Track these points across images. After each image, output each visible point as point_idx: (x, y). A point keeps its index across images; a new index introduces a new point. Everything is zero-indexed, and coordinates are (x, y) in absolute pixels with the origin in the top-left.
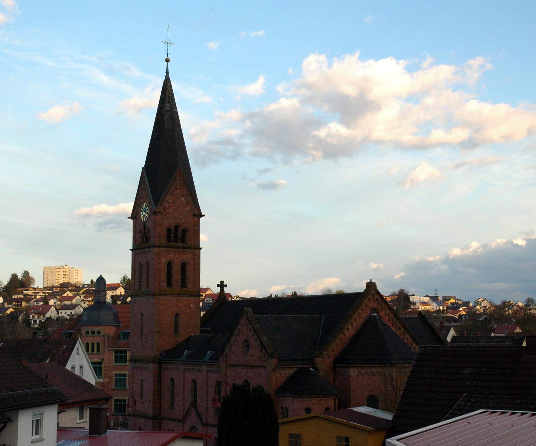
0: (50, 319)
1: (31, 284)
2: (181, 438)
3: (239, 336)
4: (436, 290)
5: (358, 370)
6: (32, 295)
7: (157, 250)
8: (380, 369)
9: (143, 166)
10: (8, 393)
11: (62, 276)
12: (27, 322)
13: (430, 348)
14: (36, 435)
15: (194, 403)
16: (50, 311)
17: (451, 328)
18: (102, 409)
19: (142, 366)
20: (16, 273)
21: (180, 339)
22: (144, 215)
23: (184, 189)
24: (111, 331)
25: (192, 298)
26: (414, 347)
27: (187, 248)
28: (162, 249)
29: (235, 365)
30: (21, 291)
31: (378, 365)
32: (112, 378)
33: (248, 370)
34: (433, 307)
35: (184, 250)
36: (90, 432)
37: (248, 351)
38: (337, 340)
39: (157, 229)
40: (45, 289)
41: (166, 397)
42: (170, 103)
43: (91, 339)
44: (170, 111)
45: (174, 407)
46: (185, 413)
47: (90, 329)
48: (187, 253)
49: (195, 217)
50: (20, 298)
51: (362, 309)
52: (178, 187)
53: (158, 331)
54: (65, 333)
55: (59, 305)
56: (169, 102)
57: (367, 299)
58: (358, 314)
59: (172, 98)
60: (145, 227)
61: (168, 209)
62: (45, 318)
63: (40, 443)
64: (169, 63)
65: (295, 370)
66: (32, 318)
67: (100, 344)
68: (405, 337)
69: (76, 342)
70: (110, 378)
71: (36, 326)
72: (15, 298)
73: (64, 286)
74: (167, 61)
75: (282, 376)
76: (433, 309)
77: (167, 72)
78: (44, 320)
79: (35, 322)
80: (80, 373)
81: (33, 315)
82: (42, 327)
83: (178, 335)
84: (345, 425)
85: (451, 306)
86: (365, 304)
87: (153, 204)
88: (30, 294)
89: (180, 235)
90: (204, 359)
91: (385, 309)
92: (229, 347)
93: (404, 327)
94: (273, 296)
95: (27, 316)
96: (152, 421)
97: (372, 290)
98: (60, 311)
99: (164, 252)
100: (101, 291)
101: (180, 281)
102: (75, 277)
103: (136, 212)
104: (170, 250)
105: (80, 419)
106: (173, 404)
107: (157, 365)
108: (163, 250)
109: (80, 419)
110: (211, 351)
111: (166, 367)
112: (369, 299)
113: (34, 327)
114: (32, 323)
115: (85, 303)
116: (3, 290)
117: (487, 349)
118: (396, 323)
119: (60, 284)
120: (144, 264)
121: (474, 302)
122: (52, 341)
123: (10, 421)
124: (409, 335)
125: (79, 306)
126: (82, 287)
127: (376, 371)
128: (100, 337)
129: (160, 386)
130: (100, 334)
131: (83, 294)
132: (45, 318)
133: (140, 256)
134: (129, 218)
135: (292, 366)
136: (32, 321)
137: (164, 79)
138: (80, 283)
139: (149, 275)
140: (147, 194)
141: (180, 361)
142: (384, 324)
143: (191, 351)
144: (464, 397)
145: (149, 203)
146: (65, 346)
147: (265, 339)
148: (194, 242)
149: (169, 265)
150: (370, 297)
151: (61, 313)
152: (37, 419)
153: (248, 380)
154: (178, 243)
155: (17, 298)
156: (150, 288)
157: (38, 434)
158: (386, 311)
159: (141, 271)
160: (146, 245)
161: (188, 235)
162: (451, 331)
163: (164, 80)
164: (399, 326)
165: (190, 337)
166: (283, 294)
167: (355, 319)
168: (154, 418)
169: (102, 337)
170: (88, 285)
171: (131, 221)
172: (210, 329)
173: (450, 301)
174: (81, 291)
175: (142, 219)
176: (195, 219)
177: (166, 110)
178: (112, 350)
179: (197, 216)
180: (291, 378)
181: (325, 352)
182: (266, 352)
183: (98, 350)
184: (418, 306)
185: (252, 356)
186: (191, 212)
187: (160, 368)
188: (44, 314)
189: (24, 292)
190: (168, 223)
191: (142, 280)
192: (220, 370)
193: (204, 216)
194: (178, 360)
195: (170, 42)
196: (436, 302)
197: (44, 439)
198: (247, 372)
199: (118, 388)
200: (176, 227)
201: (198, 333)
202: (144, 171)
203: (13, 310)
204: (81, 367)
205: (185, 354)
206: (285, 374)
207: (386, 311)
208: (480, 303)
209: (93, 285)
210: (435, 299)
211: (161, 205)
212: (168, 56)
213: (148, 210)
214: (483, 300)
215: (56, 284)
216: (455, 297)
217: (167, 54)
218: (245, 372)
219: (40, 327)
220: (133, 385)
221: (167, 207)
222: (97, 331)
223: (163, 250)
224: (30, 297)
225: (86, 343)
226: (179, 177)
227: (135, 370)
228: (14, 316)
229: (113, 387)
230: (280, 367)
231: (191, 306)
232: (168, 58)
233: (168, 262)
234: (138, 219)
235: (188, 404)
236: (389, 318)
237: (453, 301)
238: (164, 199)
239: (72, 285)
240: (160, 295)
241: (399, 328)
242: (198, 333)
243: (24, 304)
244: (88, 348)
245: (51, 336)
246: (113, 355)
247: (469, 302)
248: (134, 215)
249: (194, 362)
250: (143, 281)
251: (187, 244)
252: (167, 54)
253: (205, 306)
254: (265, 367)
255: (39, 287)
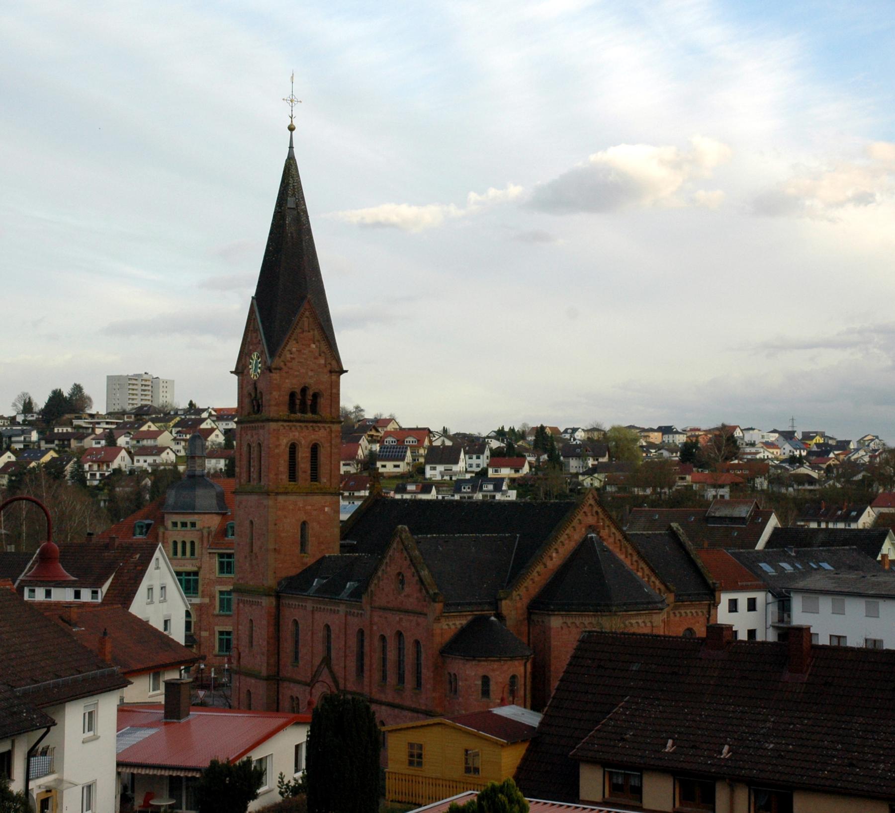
0: (118, 471)
1: (86, 407)
2: (293, 724)
3: (390, 566)
4: (793, 419)
5: (563, 619)
6: (88, 428)
7: (273, 425)
8: (593, 618)
9: (253, 295)
10: (52, 681)
11: (139, 392)
12: (79, 476)
13: (595, 634)
14: (88, 731)
15: (327, 660)
16: (119, 458)
17: (772, 514)
18: (182, 683)
19: (251, 599)
20: (59, 388)
21: (310, 560)
22: (254, 371)
23: (316, 332)
24: (214, 522)
25: (328, 498)
26: (653, 582)
27: (320, 422)
28: (280, 423)
29: (385, 609)
30: (69, 419)
31: (592, 613)
32: (214, 597)
33: (402, 616)
34: (784, 451)
35: (314, 425)
36: (166, 712)
37: (403, 588)
38: (535, 574)
39: (274, 393)
40: (109, 416)
41: (287, 646)
42: (295, 197)
43: (178, 535)
44: (294, 208)
45: (298, 663)
46: (313, 673)
47: (179, 519)
48: (320, 429)
49: (333, 374)
50: (67, 433)
51: (573, 527)
52: (307, 329)
53: (275, 549)
54: (140, 524)
55: (133, 447)
56: (294, 195)
57: (582, 512)
58: (567, 534)
59: (298, 188)
60: (256, 389)
61: (291, 362)
62: (109, 470)
63: (95, 742)
64: (294, 132)
65: (470, 618)
66: (87, 470)
67: (196, 544)
68: (640, 567)
69: (155, 550)
70: (212, 597)
71: (96, 483)
72: (58, 433)
73: (142, 414)
74: (291, 129)
75: (450, 628)
76: (784, 454)
77: (291, 147)
78: (109, 473)
79: (93, 475)
80: (162, 597)
81: (90, 463)
82: (105, 485)
83: (305, 553)
84: (474, 735)
85: (816, 449)
86: (579, 520)
87: (268, 355)
88: (84, 425)
89: (309, 403)
90: (341, 596)
91: (608, 526)
92: (375, 582)
93: (638, 553)
94: (506, 429)
95: (80, 465)
96: (265, 682)
97: (589, 498)
98: (136, 458)
99: (285, 428)
100: (197, 458)
101: (309, 472)
102: (161, 394)
103: (243, 365)
104: (295, 426)
105: (154, 690)
106: (296, 658)
107: (273, 600)
108: (282, 425)
109: (154, 690)
110: (352, 583)
111: (287, 602)
112: (585, 512)
113: (91, 485)
114: (89, 477)
115: (178, 443)
116: (37, 417)
117: (663, 638)
118: (626, 548)
119: (136, 409)
120: (254, 445)
121: (857, 442)
122: (118, 547)
123: (54, 724)
124: (646, 564)
125: (168, 450)
126: (174, 415)
127: (588, 622)
128: (196, 532)
129: (279, 631)
130: (195, 527)
131: (175, 426)
132: (109, 470)
133: (249, 432)
134: (232, 372)
135: (465, 613)
136: (89, 475)
137: (286, 158)
138: (171, 405)
139: (262, 463)
140: (259, 338)
141: (307, 596)
142: (605, 550)
143: (325, 581)
144: (625, 702)
145: (262, 353)
146: (138, 556)
147: (426, 572)
148: (331, 414)
149: (293, 449)
150: (586, 509)
151: (138, 461)
152: (90, 711)
153: (402, 631)
154: (306, 413)
155: (62, 433)
156: (263, 483)
157: (91, 730)
158: (610, 530)
159: (250, 455)
160: (258, 416)
161: (322, 401)
162: (771, 519)
163: (287, 160)
164: (630, 551)
165: (324, 558)
166: (525, 425)
167: (561, 542)
168: (268, 679)
169: (198, 533)
170: (184, 410)
171: (235, 378)
172: (355, 543)
173: (814, 441)
174: (173, 422)
175: (252, 376)
176: (333, 377)
177: (288, 208)
178: (215, 553)
179: (336, 372)
180: (463, 633)
181: (514, 592)
182: (427, 592)
183: (193, 553)
184: (757, 449)
185: (408, 596)
186: (326, 366)
187: (278, 607)
188: (108, 463)
189: (73, 421)
190: (291, 383)
191: (252, 469)
192: (363, 612)
193: (346, 371)
194: (304, 594)
195: (295, 100)
196: (790, 442)
197: (99, 737)
198: (401, 619)
199: (224, 613)
200: (304, 390)
201: (335, 551)
202: (255, 302)
203: (55, 455)
204: (163, 588)
205: (314, 584)
206: (454, 624)
207: (610, 530)
208: (867, 444)
209: (192, 411)
210: (788, 436)
211: (280, 357)
212: (292, 121)
213: (260, 363)
214: (872, 438)
215: (128, 408)
216: (824, 432)
217: (292, 118)
218: (398, 619)
219: (101, 485)
220: (238, 627)
221: (289, 359)
222: (191, 523)
223: (282, 425)
224: (85, 431)
225: (172, 541)
226: (307, 313)
227: (241, 605)
228: (55, 470)
229: (217, 611)
230: (447, 614)
231: (326, 509)
232: (292, 124)
233: (290, 443)
234: (246, 375)
235: (317, 661)
236: (615, 539)
237: (819, 440)
238: (284, 348)
239: (157, 411)
240: (277, 494)
241: (631, 554)
242: (335, 551)
243: (74, 444)
244: (176, 551)
245: (116, 540)
246: (217, 562)
247: (848, 442)
248: (240, 368)
249: (327, 598)
250: (253, 472)
251: (321, 416)
252: (292, 118)
253: (383, 452)
254: (426, 615)
255: (100, 413)
